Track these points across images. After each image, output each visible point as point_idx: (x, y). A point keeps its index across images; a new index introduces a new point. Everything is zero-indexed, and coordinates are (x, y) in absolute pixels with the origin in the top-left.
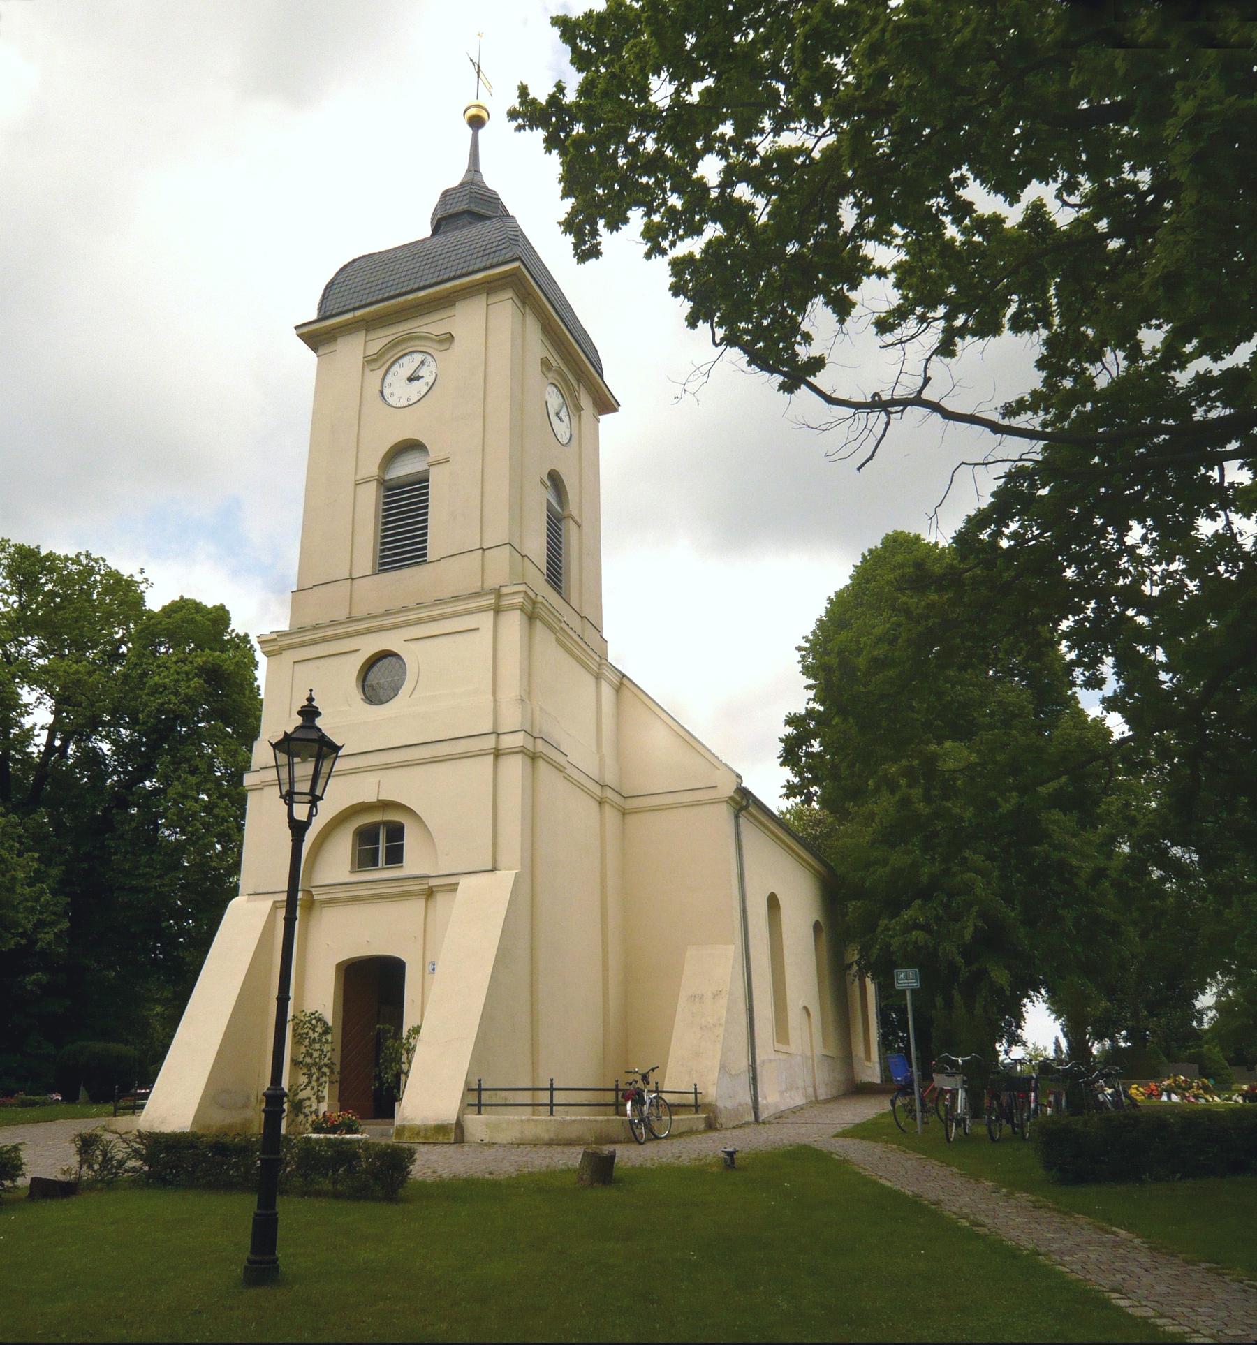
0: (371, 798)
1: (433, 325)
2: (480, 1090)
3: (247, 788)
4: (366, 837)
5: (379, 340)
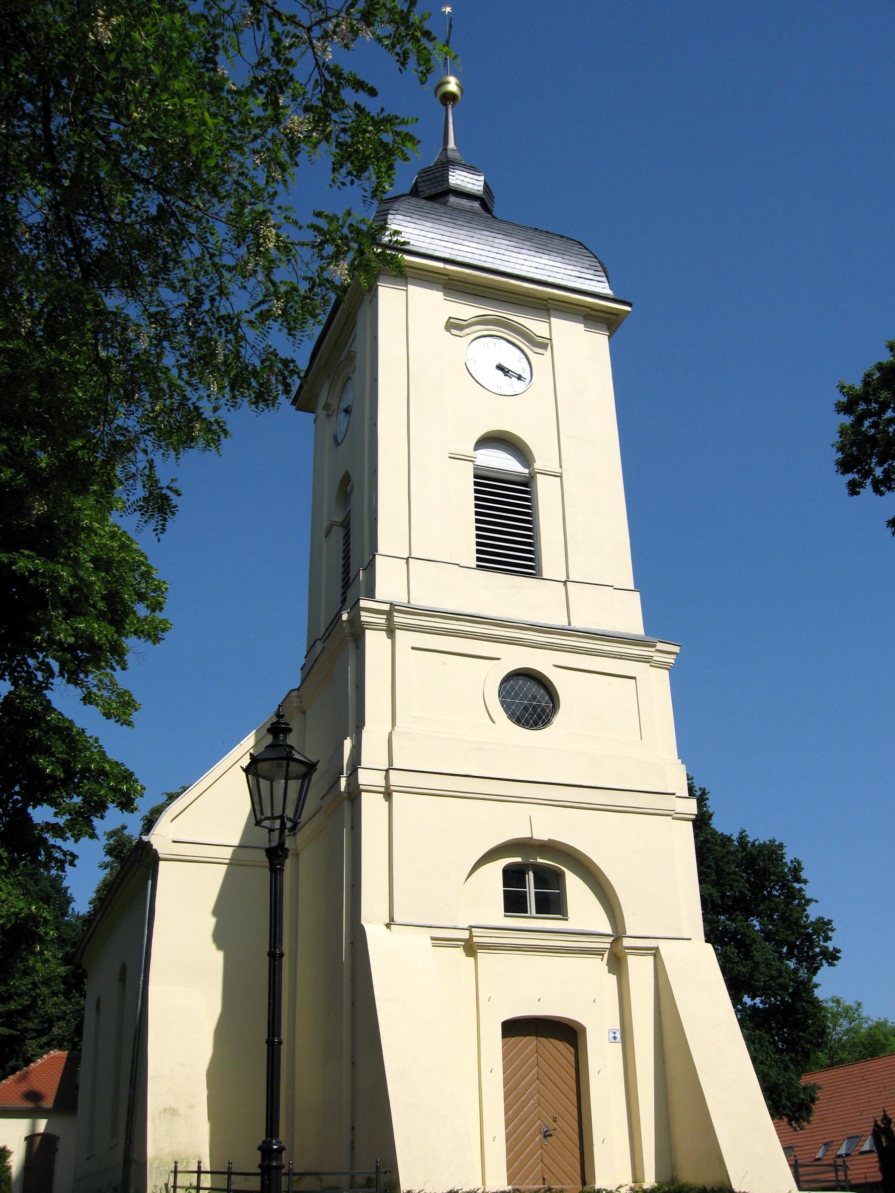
0: (542, 834)
1: (536, 326)
2: (229, 1173)
3: (361, 787)
4: (513, 876)
5: (466, 311)
